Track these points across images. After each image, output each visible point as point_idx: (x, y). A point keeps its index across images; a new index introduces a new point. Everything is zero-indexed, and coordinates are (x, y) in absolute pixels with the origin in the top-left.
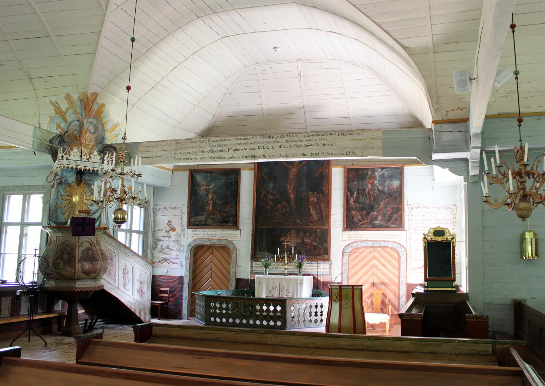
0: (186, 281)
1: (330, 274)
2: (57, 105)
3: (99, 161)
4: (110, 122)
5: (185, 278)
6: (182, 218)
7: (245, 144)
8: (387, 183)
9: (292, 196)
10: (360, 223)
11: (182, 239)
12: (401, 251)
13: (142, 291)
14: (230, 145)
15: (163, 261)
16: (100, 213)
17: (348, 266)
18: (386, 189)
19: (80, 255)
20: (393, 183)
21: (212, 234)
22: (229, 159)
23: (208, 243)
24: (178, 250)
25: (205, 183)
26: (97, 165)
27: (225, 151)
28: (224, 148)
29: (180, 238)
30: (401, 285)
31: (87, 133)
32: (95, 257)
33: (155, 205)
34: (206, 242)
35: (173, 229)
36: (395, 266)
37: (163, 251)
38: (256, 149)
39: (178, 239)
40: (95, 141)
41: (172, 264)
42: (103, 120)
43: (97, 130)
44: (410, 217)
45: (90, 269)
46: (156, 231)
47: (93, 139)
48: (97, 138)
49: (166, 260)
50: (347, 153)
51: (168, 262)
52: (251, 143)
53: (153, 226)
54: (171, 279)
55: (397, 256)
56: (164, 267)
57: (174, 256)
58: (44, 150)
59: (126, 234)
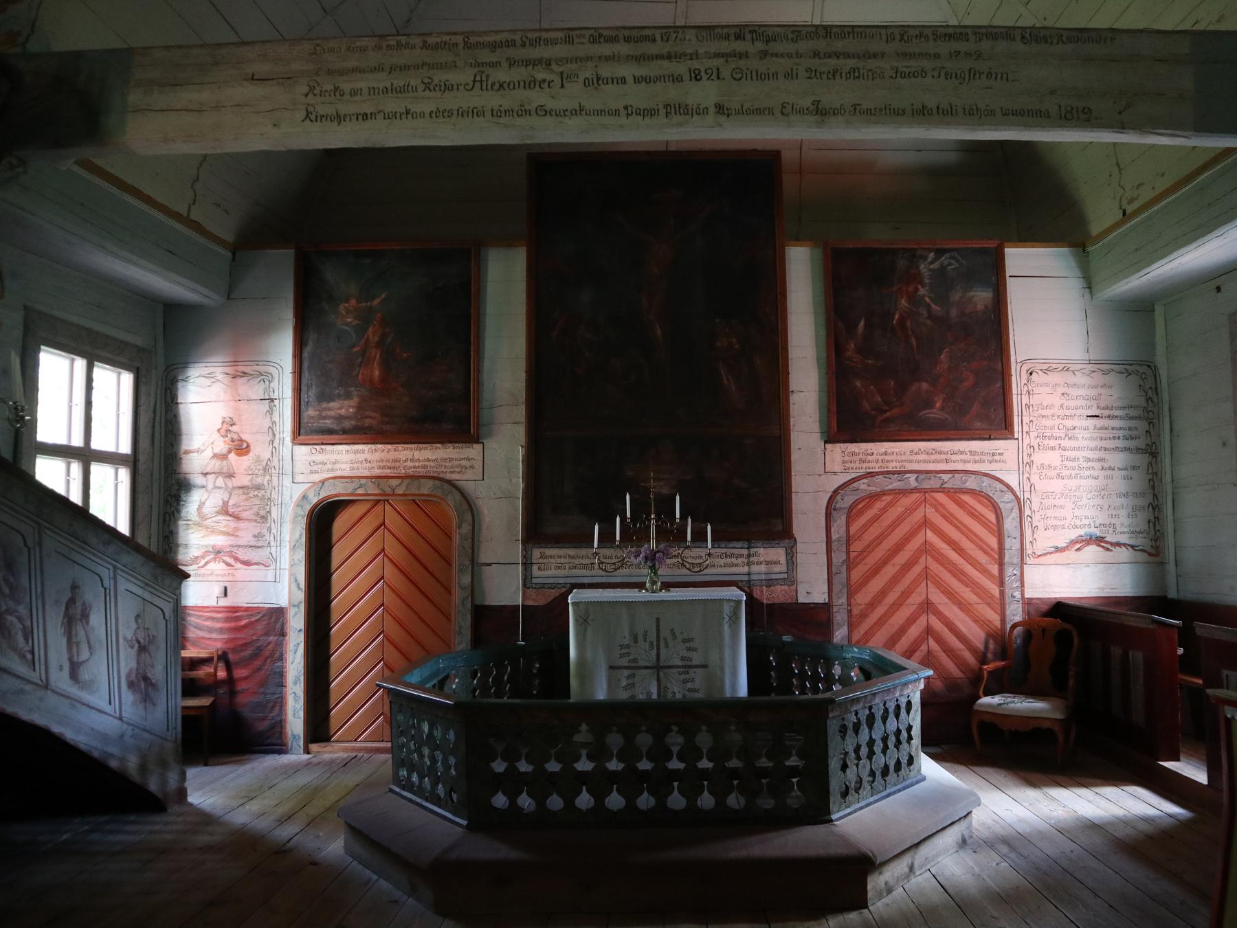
1: (791, 579)
7: (639, 59)
8: (956, 296)
9: (659, 332)
10: (880, 418)
11: (275, 479)
12: (1004, 502)
14: (567, 60)
15: (207, 559)
17: (848, 552)
18: (954, 313)
20: (973, 297)
24: (263, 517)
27: (546, 85)
29: (268, 478)
30: (1010, 604)
34: (361, 486)
36: (988, 546)
37: (208, 522)
38: (686, 77)
39: (259, 480)
41: (239, 565)
44: (1025, 400)
49: (219, 552)
50: (1063, 112)
55: (992, 517)
56: (210, 578)
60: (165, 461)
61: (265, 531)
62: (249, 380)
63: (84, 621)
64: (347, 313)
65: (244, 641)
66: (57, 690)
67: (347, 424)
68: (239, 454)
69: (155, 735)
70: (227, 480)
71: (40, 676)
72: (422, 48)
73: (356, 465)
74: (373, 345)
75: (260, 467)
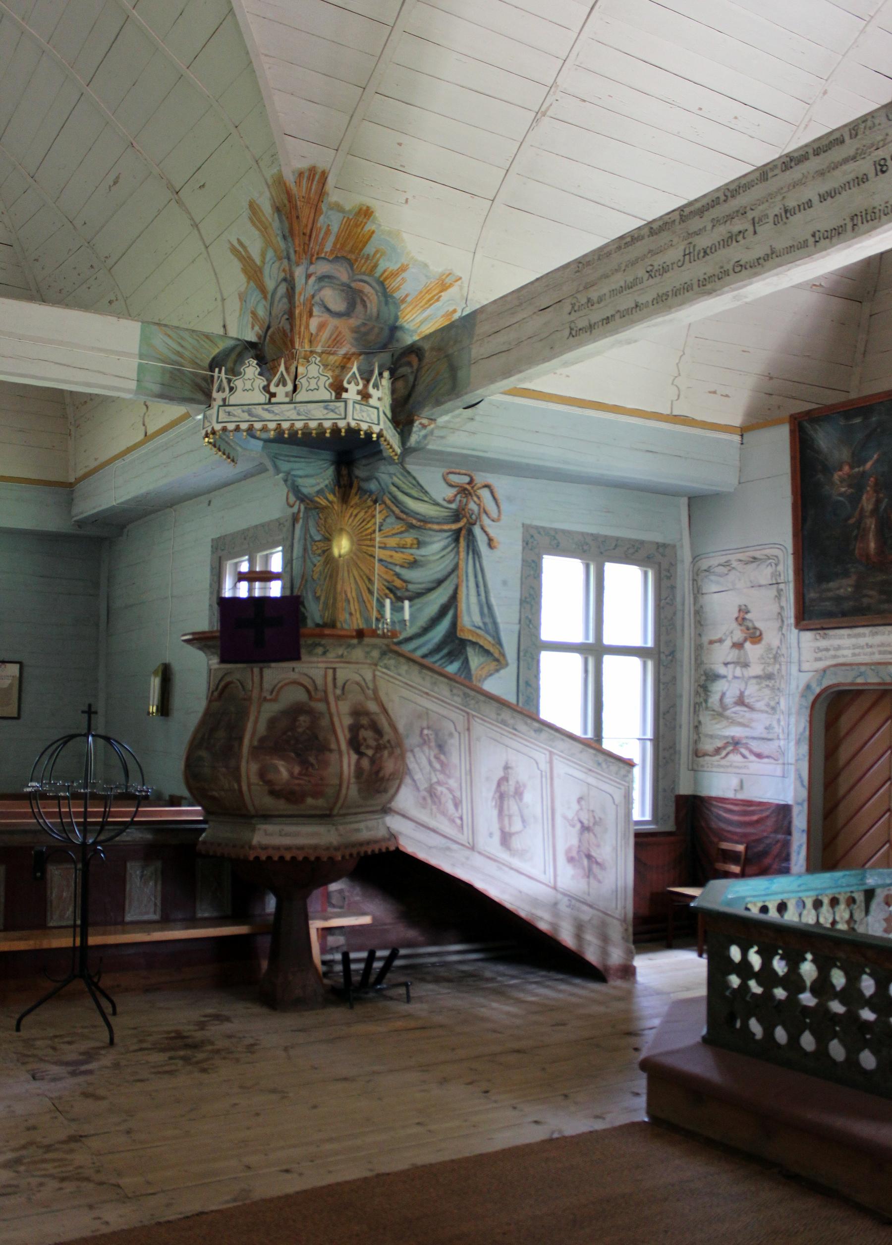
0: (800, 821)
2: (243, 253)
3: (326, 395)
4: (412, 270)
5: (795, 811)
6: (779, 596)
11: (784, 667)
13: (589, 857)
16: (450, 592)
19: (262, 728)
21: (882, 645)
22: (759, 269)
23: (870, 681)
25: (844, 454)
26: (318, 412)
27: (740, 238)
28: (737, 226)
29: (777, 666)
31: (311, 314)
32: (317, 738)
33: (695, 558)
34: (861, 674)
35: (755, 636)
39: (770, 669)
40: (356, 339)
41: (752, 758)
42: (376, 266)
43: (358, 301)
45: (297, 782)
46: (706, 644)
47: (348, 335)
48: (363, 329)
51: (743, 751)
52: (846, 161)
53: (696, 627)
54: (753, 813)
56: (729, 770)
57: (759, 730)
58: (187, 393)
59: (214, 638)
60: (695, 652)
61: (775, 724)
62: (759, 565)
63: (517, 798)
64: (841, 482)
65: (757, 837)
66: (484, 853)
67: (848, 605)
68: (753, 643)
69: (598, 910)
70: (744, 669)
71: (468, 839)
72: (649, 236)
73: (857, 651)
74: (867, 514)
75: (771, 656)
